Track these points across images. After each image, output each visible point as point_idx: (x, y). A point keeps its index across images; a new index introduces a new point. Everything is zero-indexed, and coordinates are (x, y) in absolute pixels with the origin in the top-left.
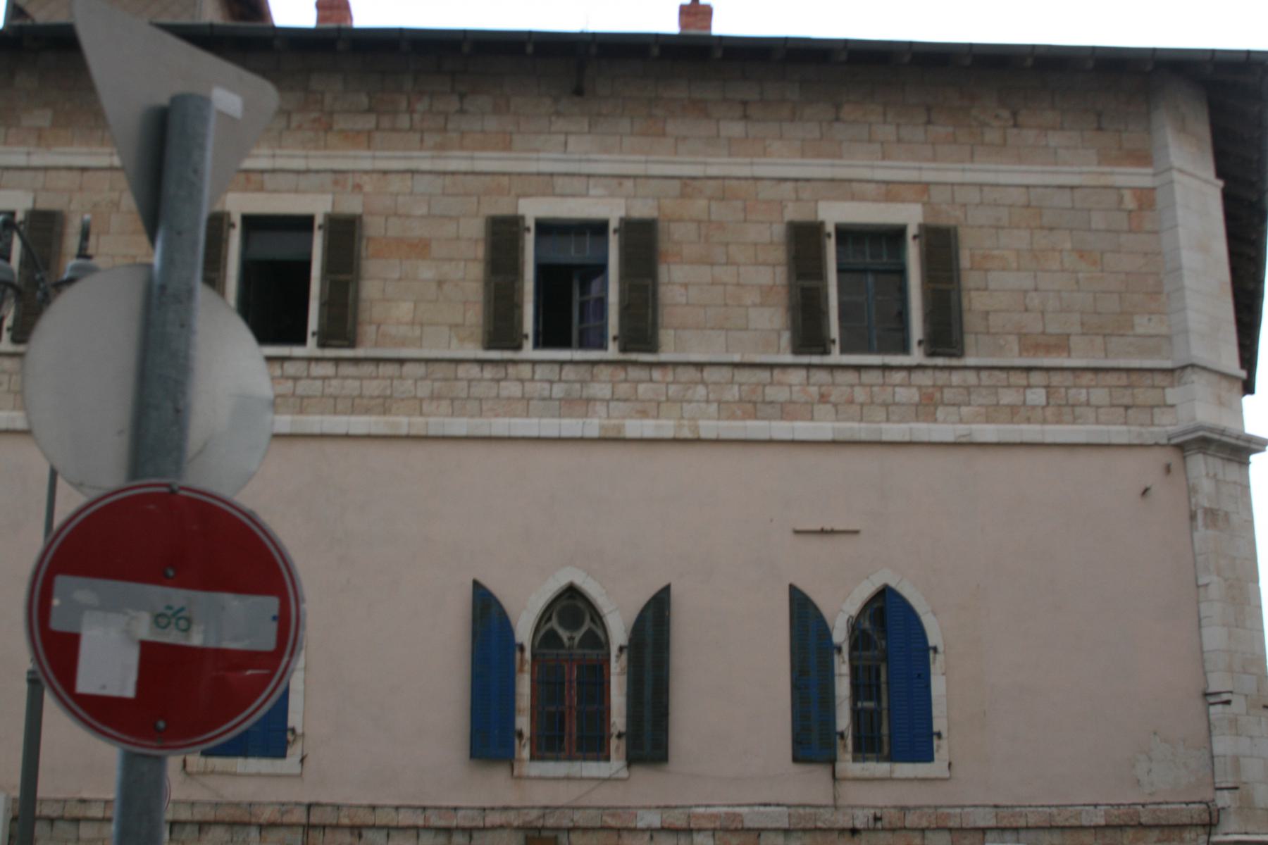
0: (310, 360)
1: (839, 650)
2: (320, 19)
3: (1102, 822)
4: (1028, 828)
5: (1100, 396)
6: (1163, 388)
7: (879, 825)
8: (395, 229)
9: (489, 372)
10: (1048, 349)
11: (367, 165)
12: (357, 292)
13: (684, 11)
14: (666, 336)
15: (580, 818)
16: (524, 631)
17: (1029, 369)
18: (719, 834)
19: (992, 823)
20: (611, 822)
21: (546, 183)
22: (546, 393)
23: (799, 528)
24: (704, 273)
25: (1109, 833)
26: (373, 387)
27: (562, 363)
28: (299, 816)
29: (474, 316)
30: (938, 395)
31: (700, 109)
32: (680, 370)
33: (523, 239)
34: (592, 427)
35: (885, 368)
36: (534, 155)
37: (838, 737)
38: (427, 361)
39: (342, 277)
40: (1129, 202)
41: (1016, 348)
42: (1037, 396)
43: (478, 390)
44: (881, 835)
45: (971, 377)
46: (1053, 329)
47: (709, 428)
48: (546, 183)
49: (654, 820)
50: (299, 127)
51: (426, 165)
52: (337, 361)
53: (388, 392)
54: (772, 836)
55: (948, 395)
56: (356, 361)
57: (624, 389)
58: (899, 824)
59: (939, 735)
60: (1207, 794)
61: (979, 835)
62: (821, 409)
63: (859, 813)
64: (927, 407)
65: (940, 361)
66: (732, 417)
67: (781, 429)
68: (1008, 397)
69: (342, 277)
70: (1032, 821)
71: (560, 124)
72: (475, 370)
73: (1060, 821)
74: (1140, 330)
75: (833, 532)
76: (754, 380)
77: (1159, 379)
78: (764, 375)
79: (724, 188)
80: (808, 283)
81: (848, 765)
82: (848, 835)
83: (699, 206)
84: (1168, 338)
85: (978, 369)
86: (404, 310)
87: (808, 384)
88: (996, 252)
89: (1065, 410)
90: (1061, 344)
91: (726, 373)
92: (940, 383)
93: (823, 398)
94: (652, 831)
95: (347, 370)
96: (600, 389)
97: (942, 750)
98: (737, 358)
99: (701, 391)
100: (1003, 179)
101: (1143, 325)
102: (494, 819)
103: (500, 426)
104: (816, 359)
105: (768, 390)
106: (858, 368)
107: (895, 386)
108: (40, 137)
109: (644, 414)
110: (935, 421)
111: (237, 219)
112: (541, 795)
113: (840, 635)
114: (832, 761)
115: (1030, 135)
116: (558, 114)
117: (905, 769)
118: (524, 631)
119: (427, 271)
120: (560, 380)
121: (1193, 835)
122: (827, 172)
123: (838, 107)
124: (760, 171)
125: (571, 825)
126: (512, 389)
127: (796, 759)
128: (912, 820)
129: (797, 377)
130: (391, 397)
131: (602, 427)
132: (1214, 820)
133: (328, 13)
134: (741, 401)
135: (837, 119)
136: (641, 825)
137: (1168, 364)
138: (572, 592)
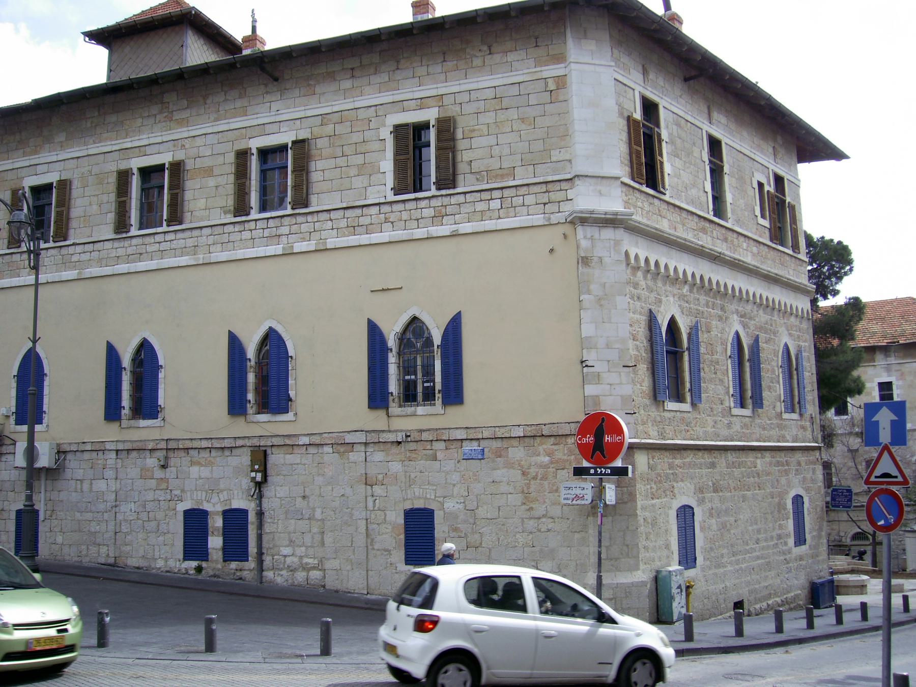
0: (165, 233)
1: (391, 350)
2: (109, 77)
3: (523, 435)
5: (530, 200)
7: (409, 439)
8: (199, 163)
9: (237, 228)
11: (185, 135)
12: (183, 196)
13: (415, 6)
14: (313, 199)
16: (251, 352)
18: (335, 446)
19: (464, 437)
21: (141, 150)
23: (372, 290)
24: (331, 163)
25: (527, 440)
26: (190, 242)
27: (268, 219)
28: (163, 445)
29: (230, 202)
30: (444, 210)
31: (331, 76)
32: (320, 214)
33: (132, 179)
34: (278, 249)
35: (416, 199)
36: (255, 116)
37: (390, 395)
38: (211, 226)
39: (124, 199)
40: (552, 86)
42: (495, 204)
43: (232, 238)
44: (411, 444)
45: (461, 198)
46: (505, 165)
48: (141, 150)
49: (305, 440)
50: (159, 122)
51: (210, 130)
52: (175, 231)
53: (196, 244)
54: (358, 446)
55: (449, 210)
56: (183, 230)
57: (295, 228)
58: (419, 439)
61: (460, 443)
62: (385, 226)
63: (400, 434)
64: (438, 217)
65: (444, 192)
67: (364, 239)
68: (481, 206)
69: (124, 199)
71: (268, 98)
72: (230, 228)
74: (554, 159)
75: (388, 289)
76: (354, 215)
77: (564, 185)
78: (358, 212)
79: (341, 117)
81: (394, 409)
82: (395, 444)
83: (329, 129)
84: (570, 161)
85: (465, 193)
86: (202, 203)
87: (380, 214)
88: (476, 127)
89: (509, 209)
91: (341, 213)
95: (180, 235)
96: (285, 230)
98: (345, 205)
100: (481, 85)
101: (556, 155)
102: (240, 443)
103: (240, 254)
106: (404, 201)
107: (421, 209)
108: (62, 147)
109: (303, 240)
112: (257, 431)
113: (392, 342)
114: (387, 408)
115: (497, 58)
116: (267, 93)
118: (251, 352)
119: (211, 182)
120: (268, 228)
122: (390, 99)
123: (398, 62)
124: (357, 105)
125: (271, 444)
126: (247, 235)
127: (105, 420)
130: (197, 246)
131: (283, 248)
133: (418, 9)
135: (398, 69)
136: (301, 443)
137: (568, 176)
138: (415, 319)
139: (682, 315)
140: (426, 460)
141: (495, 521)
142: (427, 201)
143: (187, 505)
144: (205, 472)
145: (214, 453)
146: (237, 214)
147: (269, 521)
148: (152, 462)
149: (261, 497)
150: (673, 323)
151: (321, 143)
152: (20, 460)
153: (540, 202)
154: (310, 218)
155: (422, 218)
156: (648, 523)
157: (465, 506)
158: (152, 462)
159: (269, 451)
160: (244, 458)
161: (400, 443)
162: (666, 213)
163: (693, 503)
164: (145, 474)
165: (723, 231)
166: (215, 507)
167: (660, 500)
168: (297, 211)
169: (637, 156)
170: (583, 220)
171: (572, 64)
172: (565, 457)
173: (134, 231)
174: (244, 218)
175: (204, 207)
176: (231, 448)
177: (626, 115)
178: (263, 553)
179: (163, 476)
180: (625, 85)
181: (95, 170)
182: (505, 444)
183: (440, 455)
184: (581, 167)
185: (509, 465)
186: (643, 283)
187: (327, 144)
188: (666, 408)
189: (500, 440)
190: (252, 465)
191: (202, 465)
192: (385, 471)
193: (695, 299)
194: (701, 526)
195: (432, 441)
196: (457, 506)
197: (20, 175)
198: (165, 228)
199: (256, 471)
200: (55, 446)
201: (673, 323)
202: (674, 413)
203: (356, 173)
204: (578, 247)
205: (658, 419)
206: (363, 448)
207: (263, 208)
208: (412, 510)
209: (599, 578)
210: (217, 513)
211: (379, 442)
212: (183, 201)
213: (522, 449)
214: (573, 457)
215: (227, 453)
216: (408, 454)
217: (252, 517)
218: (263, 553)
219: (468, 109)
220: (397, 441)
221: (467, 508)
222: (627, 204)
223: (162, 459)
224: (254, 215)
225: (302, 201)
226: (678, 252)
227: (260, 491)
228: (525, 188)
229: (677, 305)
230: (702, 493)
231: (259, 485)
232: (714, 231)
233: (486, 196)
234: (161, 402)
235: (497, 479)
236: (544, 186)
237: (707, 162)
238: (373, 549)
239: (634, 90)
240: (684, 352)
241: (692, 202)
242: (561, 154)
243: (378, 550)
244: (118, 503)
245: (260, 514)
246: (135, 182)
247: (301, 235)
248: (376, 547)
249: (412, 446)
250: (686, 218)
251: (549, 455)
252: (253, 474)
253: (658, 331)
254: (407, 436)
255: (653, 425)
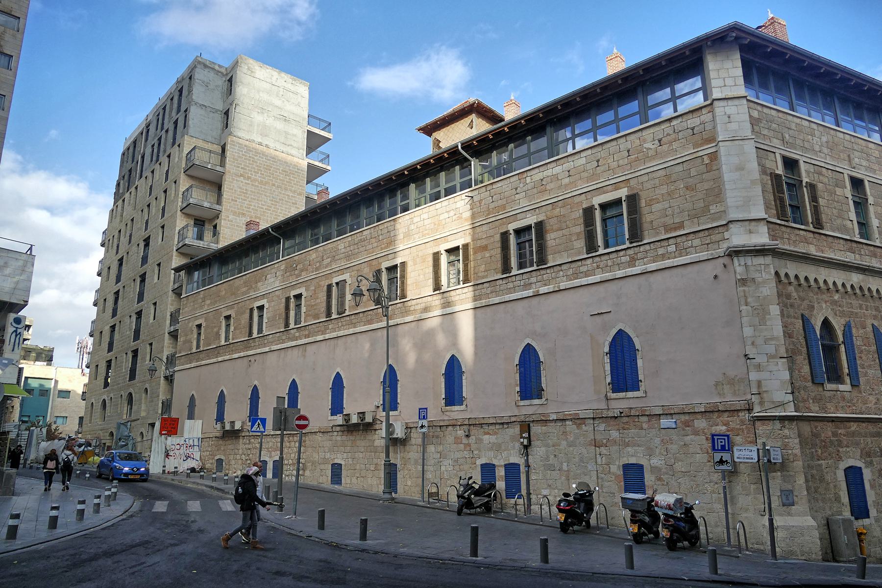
3: (704, 410)
4: (675, 414)
5: (697, 242)
6: (723, 233)
10: (675, 229)
15: (535, 418)
17: (668, 239)
20: (544, 419)
22: (519, 285)
24: (560, 233)
25: (707, 414)
29: (499, 265)
30: (636, 257)
32: (555, 268)
34: (530, 292)
35: (616, 251)
41: (663, 232)
42: (672, 248)
44: (624, 418)
45: (647, 247)
47: (563, 286)
49: (554, 417)
55: (639, 255)
59: (641, 381)
60: (749, 397)
61: (658, 417)
64: (632, 262)
65: (635, 244)
66: (571, 280)
68: (661, 251)
69: (633, 216)
70: (676, 411)
72: (500, 282)
73: (686, 410)
74: (712, 212)
75: (602, 313)
78: (580, 263)
80: (540, 242)
84: (725, 211)
89: (682, 251)
90: (681, 226)
91: (568, 265)
92: (636, 252)
93: (598, 267)
94: (555, 421)
96: (533, 280)
97: (642, 388)
99: (561, 273)
101: (713, 209)
102: (513, 419)
103: (507, 297)
104: (594, 254)
105: (581, 268)
109: (545, 285)
110: (635, 266)
111: (597, 206)
117: (630, 394)
121: (743, 414)
126: (511, 285)
128: (633, 413)
129: (589, 261)
132: (751, 408)
134: (573, 274)
136: (551, 419)
137: (724, 223)
138: (620, 332)
139: (835, 317)
140: (635, 429)
141: (688, 474)
142: (624, 252)
143: (484, 461)
144: (493, 439)
145: (497, 427)
146: (588, 252)
147: (534, 471)
148: (461, 433)
149: (527, 455)
150: (826, 323)
151: (552, 221)
152: (383, 433)
153: (704, 243)
154: (548, 271)
155: (622, 263)
156: (816, 479)
157: (666, 462)
158: (461, 433)
159: (531, 425)
160: (517, 429)
161: (616, 417)
162: (813, 240)
163: (859, 464)
164: (457, 441)
165: (872, 248)
166: (499, 462)
167: (827, 462)
168: (540, 267)
169: (780, 201)
170: (735, 253)
171: (720, 143)
172: (738, 427)
173: (515, 272)
174: (508, 275)
175: (483, 270)
176: (507, 423)
177: (769, 172)
178: (531, 494)
179: (467, 442)
180: (767, 150)
181: (420, 254)
182: (692, 417)
183: (645, 426)
184: (733, 216)
185: (696, 433)
186: (794, 294)
187: (556, 222)
188: (825, 389)
189: (688, 414)
190: (521, 434)
191: (491, 435)
192: (608, 437)
193: (847, 303)
194: (871, 485)
195: (638, 416)
196: (660, 462)
197: (380, 261)
198: (398, 301)
199: (524, 438)
200: (404, 424)
201: (826, 323)
202: (834, 392)
203: (576, 238)
204: (735, 273)
205: (818, 397)
206: (592, 421)
207: (607, 246)
208: (628, 464)
209: (771, 521)
210: (501, 466)
211: (603, 417)
212: (641, 224)
213: (704, 420)
214: (744, 427)
215: (505, 426)
216: (623, 425)
217: (523, 469)
218: (531, 494)
219: (648, 185)
220: (614, 417)
221: (667, 464)
222: (773, 237)
223: (467, 431)
224: (601, 251)
225: (542, 261)
226: (826, 269)
227: (527, 451)
228: (692, 235)
229: (830, 309)
230: (870, 456)
231: (526, 447)
232: (862, 250)
233: (665, 243)
234: (464, 395)
235: (687, 443)
236: (706, 231)
237: (850, 197)
238: (603, 492)
239: (775, 153)
240: (840, 344)
241: (839, 230)
242: (717, 208)
243: (606, 493)
244: (441, 459)
245: (528, 466)
246: (598, 214)
247: (544, 283)
248: (604, 491)
249: (625, 420)
250: (832, 243)
251: (725, 425)
252: (522, 440)
253: (811, 330)
254: (621, 413)
255: (813, 402)
